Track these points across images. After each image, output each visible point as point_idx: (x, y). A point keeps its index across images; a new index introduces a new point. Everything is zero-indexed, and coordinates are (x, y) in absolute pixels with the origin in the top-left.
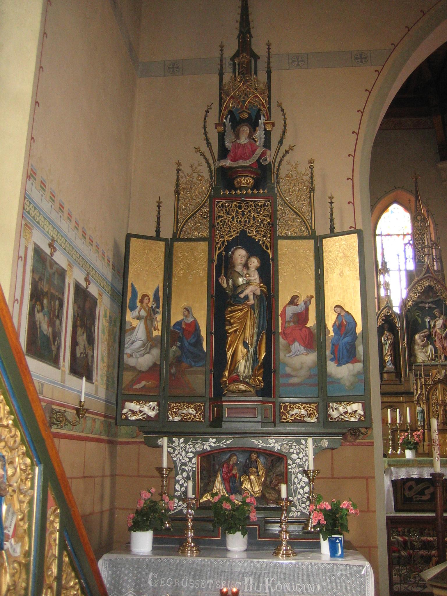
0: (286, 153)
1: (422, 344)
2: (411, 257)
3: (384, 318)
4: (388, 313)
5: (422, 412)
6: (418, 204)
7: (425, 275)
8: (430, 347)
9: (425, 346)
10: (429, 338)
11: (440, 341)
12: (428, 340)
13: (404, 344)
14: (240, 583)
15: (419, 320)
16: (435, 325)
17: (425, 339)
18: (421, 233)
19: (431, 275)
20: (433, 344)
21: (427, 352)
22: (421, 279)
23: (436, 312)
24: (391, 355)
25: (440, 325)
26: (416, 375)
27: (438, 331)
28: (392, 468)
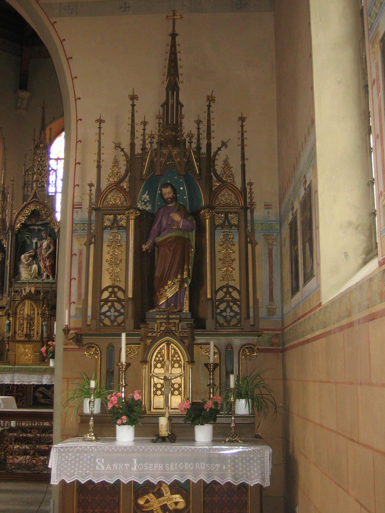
0: (198, 125)
2: (50, 186)
5: (9, 325)
9: (30, 265)
10: (35, 257)
11: (44, 260)
14: (219, 465)
15: (28, 241)
16: (41, 246)
18: (41, 160)
19: (37, 200)
20: (38, 264)
21: (30, 271)
22: (29, 204)
23: (43, 234)
27: (43, 252)
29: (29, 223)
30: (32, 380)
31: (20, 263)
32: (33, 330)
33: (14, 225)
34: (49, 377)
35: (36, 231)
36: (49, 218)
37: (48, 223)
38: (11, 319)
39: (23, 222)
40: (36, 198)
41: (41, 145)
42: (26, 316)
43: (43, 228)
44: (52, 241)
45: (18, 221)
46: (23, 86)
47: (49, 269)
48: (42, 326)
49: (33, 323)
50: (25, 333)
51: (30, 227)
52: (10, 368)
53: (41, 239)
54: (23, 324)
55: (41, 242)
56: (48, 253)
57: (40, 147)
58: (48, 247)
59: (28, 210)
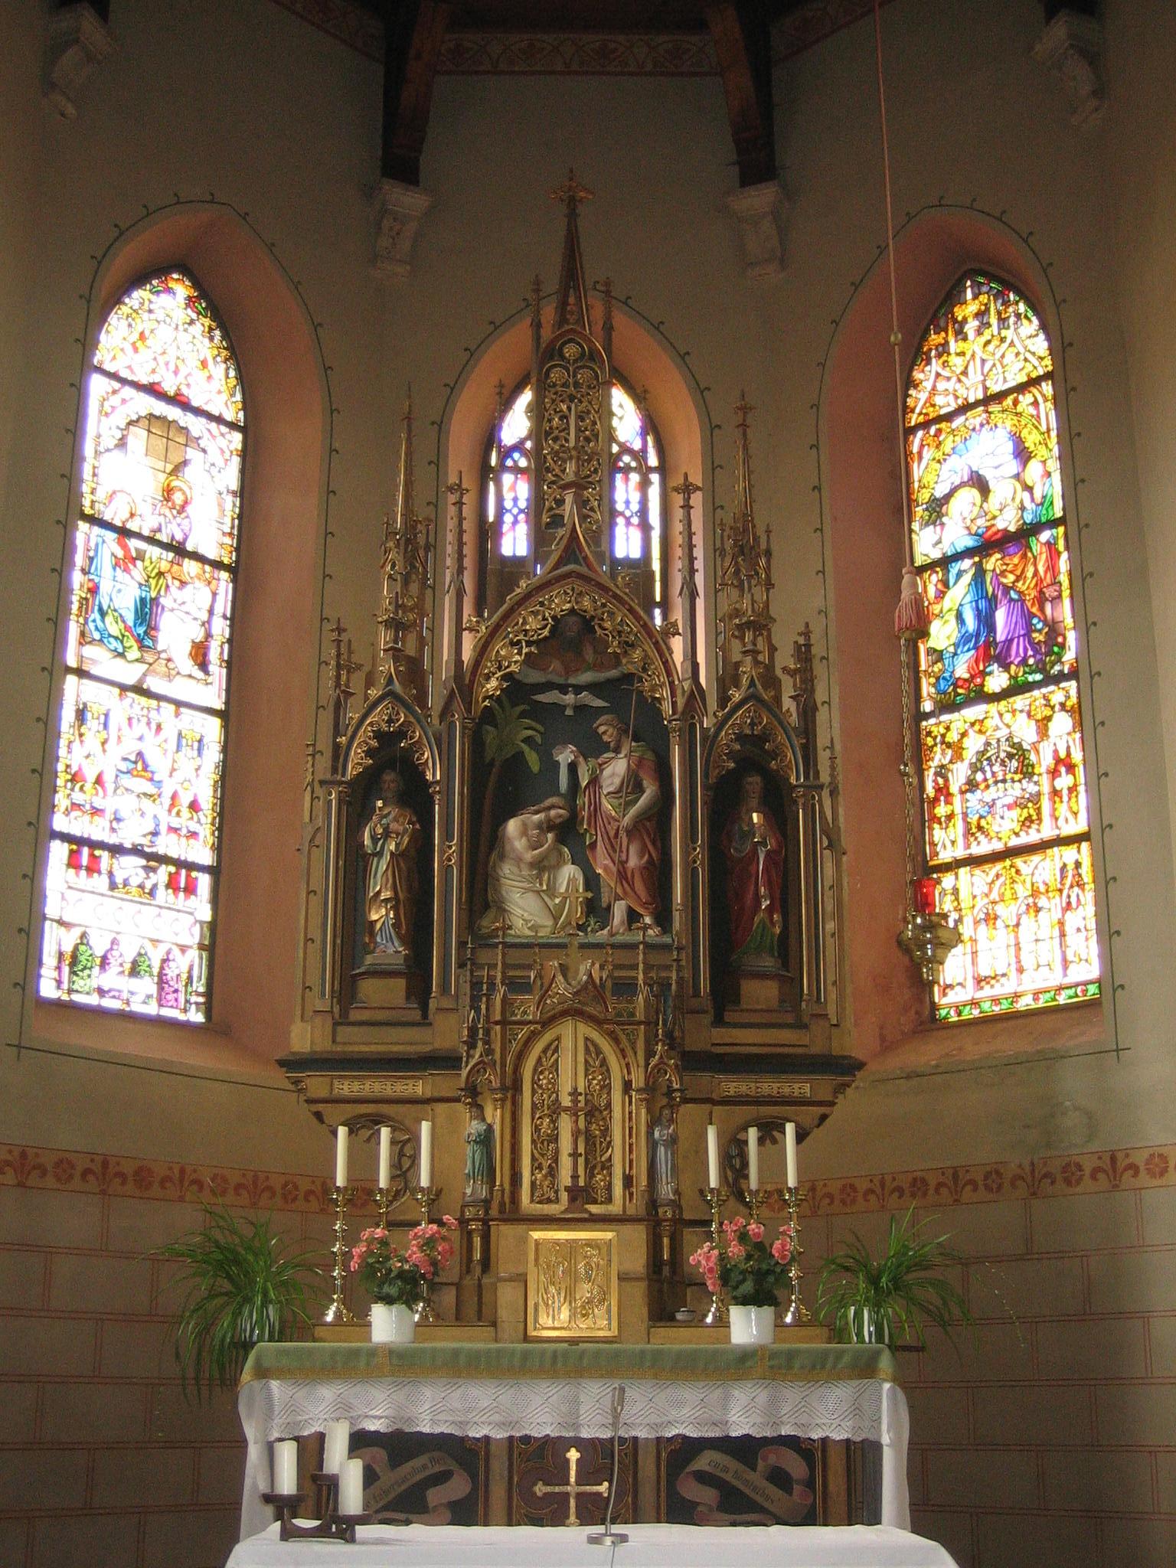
1: (529, 856)
3: (374, 743)
4: (390, 721)
5: (485, 1140)
6: (572, 300)
7: (556, 567)
8: (569, 873)
9: (542, 867)
10: (568, 833)
11: (612, 847)
12: (561, 840)
13: (448, 854)
15: (533, 760)
16: (595, 781)
17: (550, 836)
19: (584, 570)
20: (582, 861)
23: (606, 729)
24: (395, 902)
25: (617, 781)
26: (476, 985)
27: (607, 805)
28: (275, 1385)
29: (535, 677)
30: (674, 1414)
31: (502, 857)
32: (607, 1166)
33: (472, 682)
34: (762, 1396)
35: (569, 712)
36: (637, 654)
37: (628, 678)
38: (494, 1115)
39: (514, 668)
40: (577, 562)
41: (570, 351)
42: (566, 1101)
43: (599, 703)
44: (649, 755)
45: (489, 666)
46: (401, 164)
47: (639, 885)
48: (652, 1145)
49: (606, 1131)
50: (565, 1178)
51: (540, 698)
52: (555, 1353)
53: (594, 748)
54: (555, 1138)
55: (592, 762)
56: (633, 811)
57: (562, 357)
58: (633, 785)
59: (535, 613)
